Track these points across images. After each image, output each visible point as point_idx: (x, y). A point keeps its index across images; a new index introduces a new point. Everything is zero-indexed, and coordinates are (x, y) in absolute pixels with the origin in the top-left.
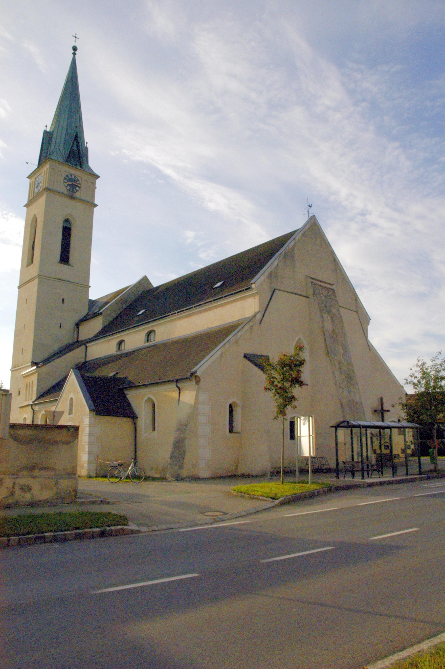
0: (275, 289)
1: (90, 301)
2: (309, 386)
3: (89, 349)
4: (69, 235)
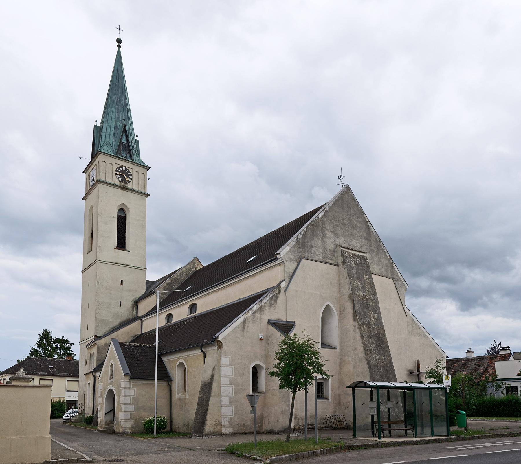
0: (99, 181)
1: (147, 281)
2: (338, 350)
3: (144, 323)
4: (125, 224)
